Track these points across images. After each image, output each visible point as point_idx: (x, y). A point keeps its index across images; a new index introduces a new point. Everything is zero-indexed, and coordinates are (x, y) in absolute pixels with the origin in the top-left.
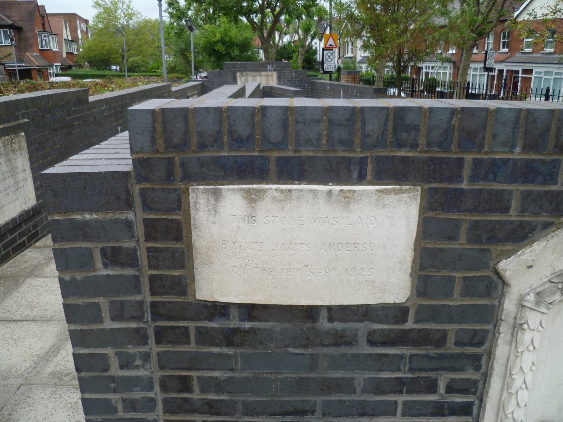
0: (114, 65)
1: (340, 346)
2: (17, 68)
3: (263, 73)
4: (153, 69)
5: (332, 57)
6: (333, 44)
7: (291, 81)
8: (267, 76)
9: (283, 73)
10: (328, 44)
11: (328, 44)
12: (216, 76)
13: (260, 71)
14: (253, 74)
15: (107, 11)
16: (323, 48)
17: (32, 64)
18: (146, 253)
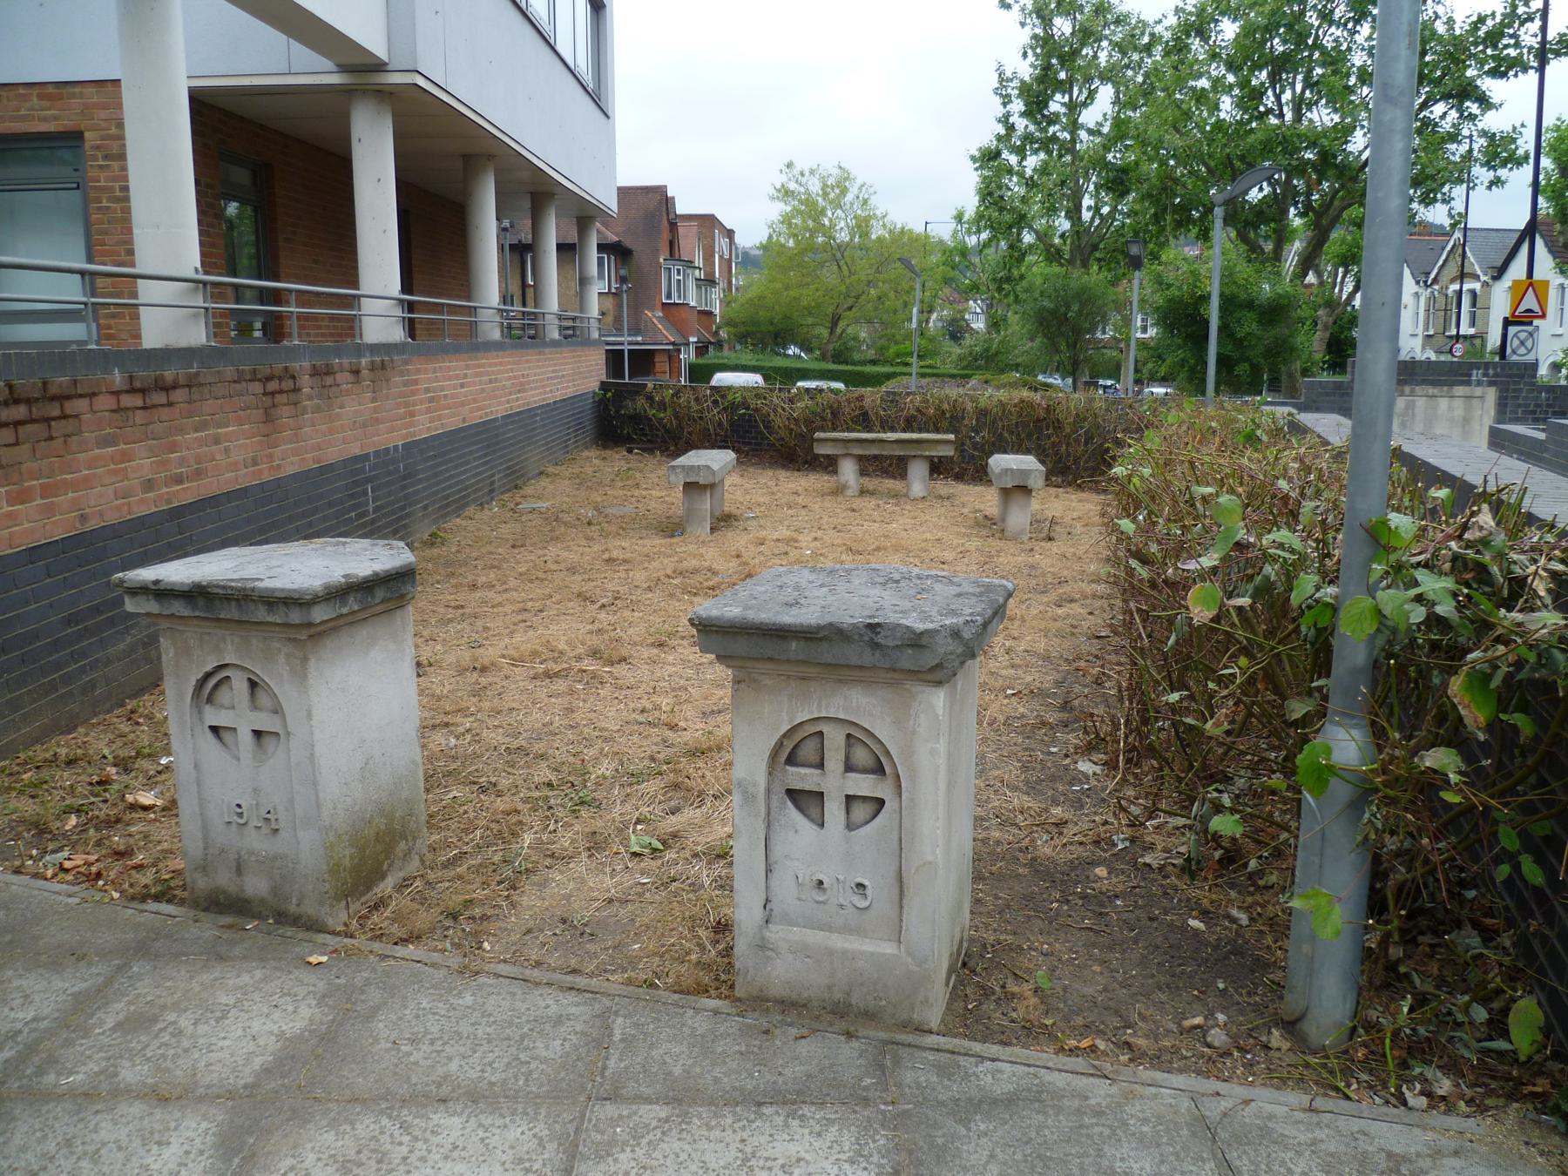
0: (795, 345)
2: (626, 348)
3: (1459, 390)
4: (898, 356)
5: (1529, 344)
6: (1536, 308)
7: (1534, 412)
8: (1468, 397)
9: (1515, 391)
10: (1522, 308)
11: (1522, 308)
12: (1327, 394)
14: (1431, 390)
15: (811, 210)
16: (1506, 319)
17: (659, 338)
18: (975, 746)
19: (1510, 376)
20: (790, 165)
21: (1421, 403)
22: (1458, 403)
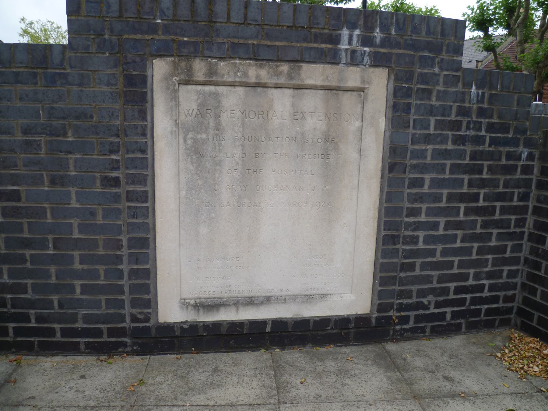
1: (218, 310)
3: (314, 73)
7: (456, 125)
9: (424, 79)
13: (298, 61)
14: (254, 72)
19: (414, 46)
20: (23, 20)
21: (232, 99)
22: (312, 102)
